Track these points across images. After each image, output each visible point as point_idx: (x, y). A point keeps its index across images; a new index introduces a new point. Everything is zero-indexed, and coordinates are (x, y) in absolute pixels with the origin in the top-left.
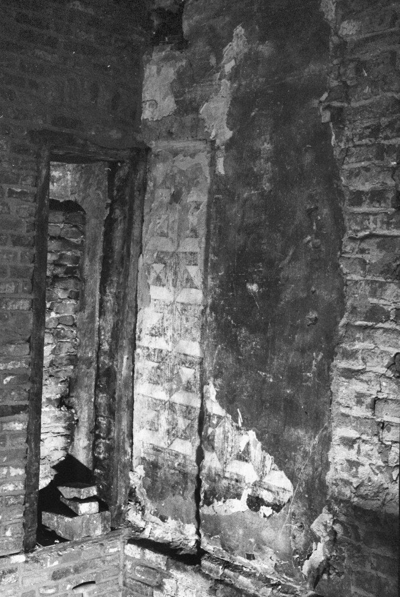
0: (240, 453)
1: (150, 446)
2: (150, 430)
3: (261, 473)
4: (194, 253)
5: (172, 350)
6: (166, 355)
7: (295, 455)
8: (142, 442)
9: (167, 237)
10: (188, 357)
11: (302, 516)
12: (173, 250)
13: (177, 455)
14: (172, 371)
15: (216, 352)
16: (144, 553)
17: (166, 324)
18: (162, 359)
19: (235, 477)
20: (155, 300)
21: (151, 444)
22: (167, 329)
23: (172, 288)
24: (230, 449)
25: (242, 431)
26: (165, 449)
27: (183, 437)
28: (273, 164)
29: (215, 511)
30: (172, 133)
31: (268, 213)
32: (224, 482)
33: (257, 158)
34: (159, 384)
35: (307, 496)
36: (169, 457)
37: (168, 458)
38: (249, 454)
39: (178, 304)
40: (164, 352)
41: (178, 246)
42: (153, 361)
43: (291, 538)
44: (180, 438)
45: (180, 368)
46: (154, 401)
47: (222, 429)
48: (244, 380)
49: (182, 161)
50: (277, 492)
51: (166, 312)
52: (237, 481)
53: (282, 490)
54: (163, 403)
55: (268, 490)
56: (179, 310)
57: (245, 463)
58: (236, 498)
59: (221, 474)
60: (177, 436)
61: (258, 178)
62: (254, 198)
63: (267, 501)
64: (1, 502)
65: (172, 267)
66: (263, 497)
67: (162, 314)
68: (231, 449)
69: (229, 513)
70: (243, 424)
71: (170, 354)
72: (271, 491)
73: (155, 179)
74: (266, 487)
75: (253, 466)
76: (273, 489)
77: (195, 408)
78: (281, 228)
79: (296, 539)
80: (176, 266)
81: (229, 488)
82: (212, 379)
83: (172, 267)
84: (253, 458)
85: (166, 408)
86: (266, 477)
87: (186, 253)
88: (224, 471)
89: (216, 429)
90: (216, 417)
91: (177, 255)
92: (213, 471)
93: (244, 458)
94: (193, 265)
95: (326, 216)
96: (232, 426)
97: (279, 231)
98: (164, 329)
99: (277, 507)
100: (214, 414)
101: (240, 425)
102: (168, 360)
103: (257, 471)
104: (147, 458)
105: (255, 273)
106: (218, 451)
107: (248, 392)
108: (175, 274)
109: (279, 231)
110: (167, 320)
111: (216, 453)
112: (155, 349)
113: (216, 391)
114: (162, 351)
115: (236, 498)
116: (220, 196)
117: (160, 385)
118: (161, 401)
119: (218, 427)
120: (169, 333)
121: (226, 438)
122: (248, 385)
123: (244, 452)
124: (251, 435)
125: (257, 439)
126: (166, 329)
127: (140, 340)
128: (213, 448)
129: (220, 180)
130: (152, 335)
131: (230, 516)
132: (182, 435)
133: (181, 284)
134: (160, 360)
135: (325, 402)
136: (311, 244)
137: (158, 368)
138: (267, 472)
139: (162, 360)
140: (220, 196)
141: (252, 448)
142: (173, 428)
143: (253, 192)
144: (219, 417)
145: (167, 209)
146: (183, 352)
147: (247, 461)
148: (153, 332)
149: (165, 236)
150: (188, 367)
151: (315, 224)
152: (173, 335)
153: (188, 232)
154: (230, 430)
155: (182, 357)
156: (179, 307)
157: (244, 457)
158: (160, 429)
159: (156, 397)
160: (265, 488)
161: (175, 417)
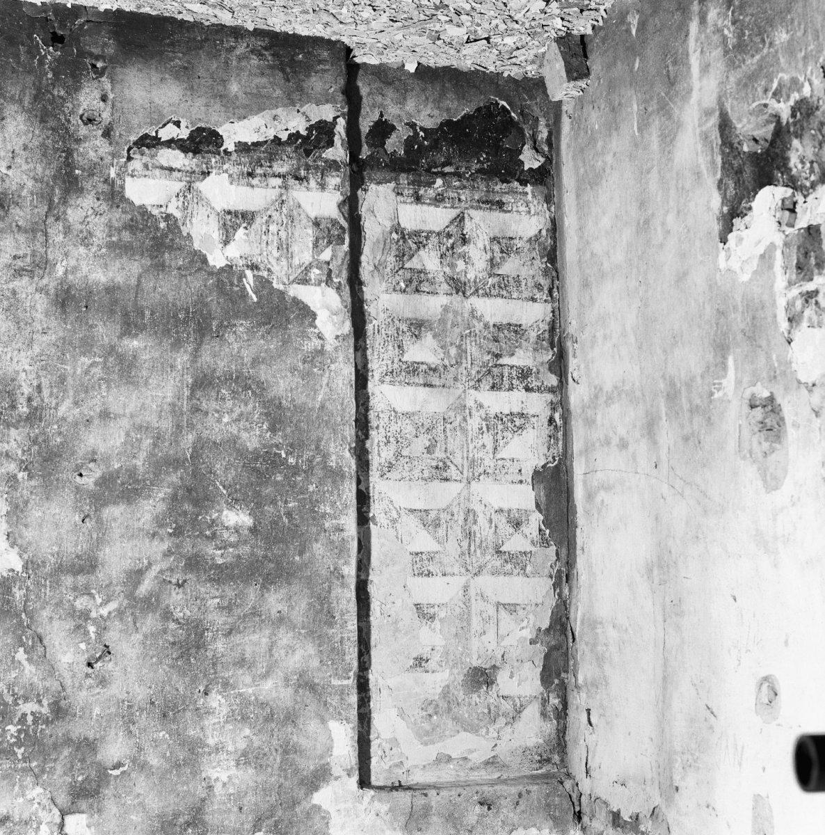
0: (245, 225)
1: (510, 209)
2: (511, 238)
3: (189, 197)
4: (420, 574)
5: (464, 391)
6: (479, 381)
7: (110, 236)
8: (532, 212)
9: (498, 604)
10: (422, 382)
11: (86, 137)
12: (479, 579)
13: (439, 200)
14: (462, 351)
15: (320, 397)
16: (216, 7)
17: (488, 439)
18: (489, 373)
19: (255, 181)
20: (521, 482)
21: (509, 212)
22: (481, 429)
23: (478, 508)
24: (273, 228)
25: (241, 263)
26: (472, 207)
27: (423, 234)
28: (200, 743)
29: (304, 114)
30: (481, 804)
31: (209, 654)
32: (281, 167)
33: (245, 754)
34: (494, 325)
35: (77, 172)
36: (459, 194)
37: (461, 192)
38: (225, 224)
39: (458, 478)
40: (486, 385)
41: (466, 589)
42: (512, 367)
43: (111, 96)
44: (431, 232)
45: (443, 360)
46: (504, 293)
47: (296, 261)
48: (245, 353)
49: (471, 751)
50: (148, 169)
51: (487, 462)
52: (250, 175)
53: (136, 173)
54: (481, 292)
55: (171, 169)
56: (453, 468)
57: (232, 209)
58: (250, 144)
59: (291, 182)
60: (439, 234)
61: (241, 716)
62: (248, 679)
63: (174, 149)
64: (3, 19)
65: (480, 547)
66: (182, 155)
67: (498, 456)
68: (271, 228)
69: (267, 114)
70: (242, 276)
71: (471, 383)
72: (162, 168)
73: (544, 714)
74: (176, 174)
75: (213, 205)
76: (157, 172)
77: (394, 290)
78: (172, 626)
79: (98, 96)
80: (469, 550)
81: (271, 160)
82: (328, 348)
83: (480, 547)
84: (213, 218)
85: (472, 284)
86: (178, 191)
87: (444, 575)
88: (285, 187)
89: (311, 259)
90: (313, 281)
91: (467, 570)
92: (313, 183)
93: (236, 216)
94: (421, 553)
95: (66, 649)
96: (269, 270)
97: (177, 621)
98: (488, 429)
99: (148, 142)
100: (319, 285)
101: (249, 273)
102: (474, 372)
103: (200, 198)
104: (516, 184)
105: (232, 545)
106: (304, 221)
107: (235, 332)
108: (470, 535)
109: (177, 621)
110: (484, 446)
111: (308, 217)
112: (511, 389)
113: (315, 327)
114: (493, 388)
115: (250, 144)
116: (336, 682)
117: (491, 324)
118: (487, 295)
119: (307, 263)
120: (474, 423)
121: (284, 248)
122: (236, 346)
123: (235, 228)
124: (217, 259)
125: (204, 252)
126: (485, 429)
127: (552, 403)
128: (317, 223)
129: (340, 714)
130: (522, 415)
131: (261, 109)
132: (427, 238)
133: (453, 515)
134: (495, 370)
135: (45, 333)
136: (99, 601)
137: (498, 356)
138: (174, 199)
139: (489, 372)
140: (336, 682)
141: (217, 235)
142: (452, 248)
143: (250, 691)
144: (304, 281)
145: (503, 656)
146: (435, 390)
147: (229, 213)
148: (518, 422)
149: (504, 605)
150: (422, 363)
151: (93, 636)
152: (465, 419)
153: (442, 615)
154: (273, 262)
155: (436, 381)
156: (452, 472)
157: (236, 220)
158: (487, 243)
159: (499, 301)
160: (179, 171)
161: (447, 270)
